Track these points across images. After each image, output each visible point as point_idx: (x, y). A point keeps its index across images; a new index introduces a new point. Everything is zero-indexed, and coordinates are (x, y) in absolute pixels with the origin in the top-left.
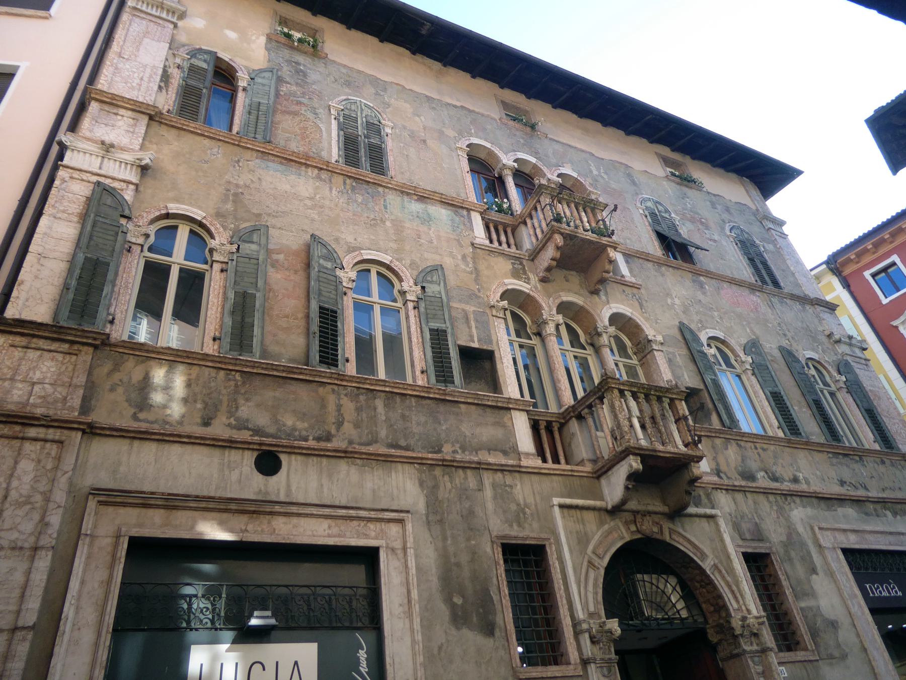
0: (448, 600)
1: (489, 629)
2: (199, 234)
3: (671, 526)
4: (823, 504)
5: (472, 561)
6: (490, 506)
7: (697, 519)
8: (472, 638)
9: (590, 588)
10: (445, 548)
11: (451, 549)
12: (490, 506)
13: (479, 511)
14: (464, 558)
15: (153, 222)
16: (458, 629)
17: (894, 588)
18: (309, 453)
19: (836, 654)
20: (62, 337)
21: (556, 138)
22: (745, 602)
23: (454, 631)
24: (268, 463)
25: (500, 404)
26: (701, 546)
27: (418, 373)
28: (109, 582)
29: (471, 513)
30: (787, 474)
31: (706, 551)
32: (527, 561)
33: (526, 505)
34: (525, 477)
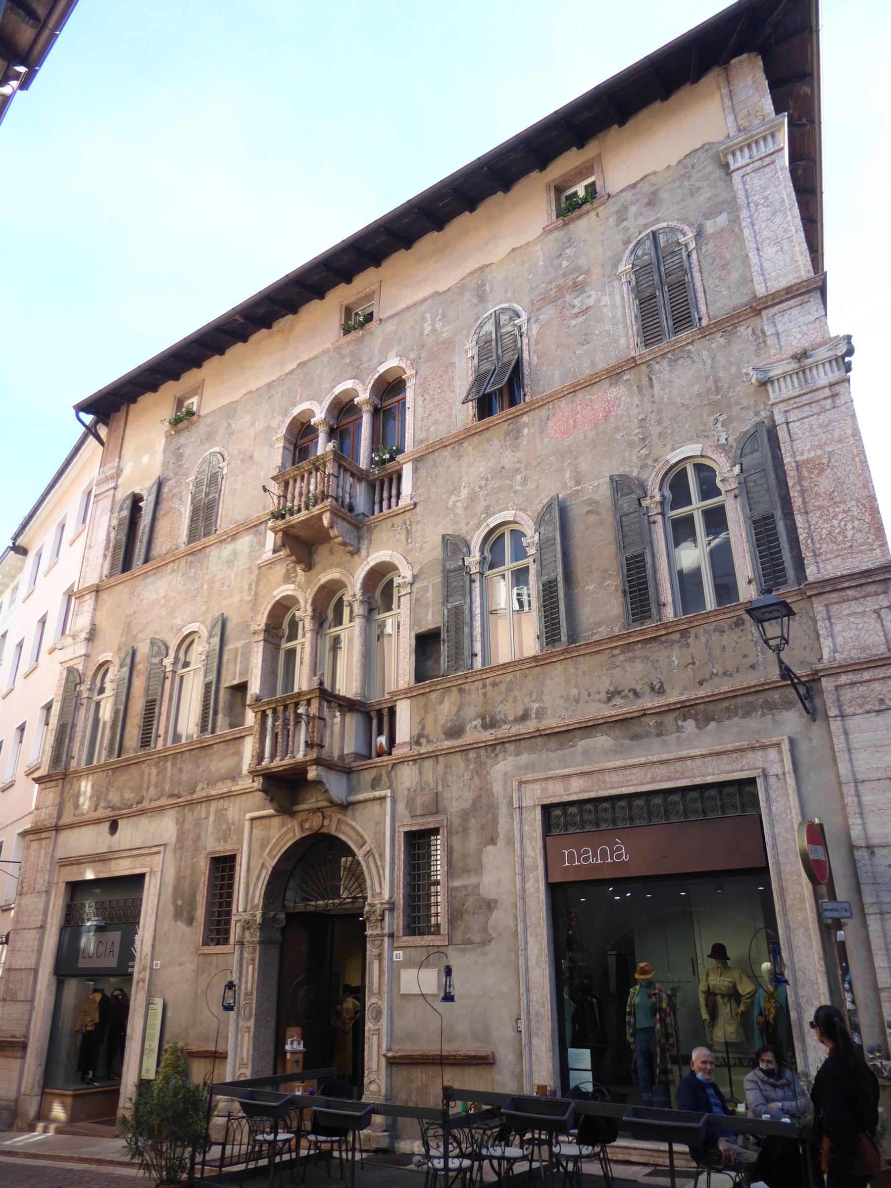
0: (175, 903)
1: (190, 921)
2: (705, 473)
3: (340, 816)
4: (553, 743)
5: (192, 873)
6: (210, 829)
7: (370, 804)
8: (181, 926)
9: (260, 885)
10: (180, 866)
11: (182, 867)
12: (210, 829)
13: (203, 836)
14: (189, 871)
15: (660, 489)
16: (176, 921)
17: (619, 849)
18: (129, 816)
19: (477, 938)
20: (838, 587)
21: (393, 312)
22: (384, 884)
23: (173, 924)
24: (114, 827)
25: (236, 736)
26: (363, 833)
27: (480, 655)
28: (772, 826)
29: (198, 837)
30: (510, 710)
31: (366, 837)
32: (223, 867)
33: (233, 824)
34: (238, 798)
